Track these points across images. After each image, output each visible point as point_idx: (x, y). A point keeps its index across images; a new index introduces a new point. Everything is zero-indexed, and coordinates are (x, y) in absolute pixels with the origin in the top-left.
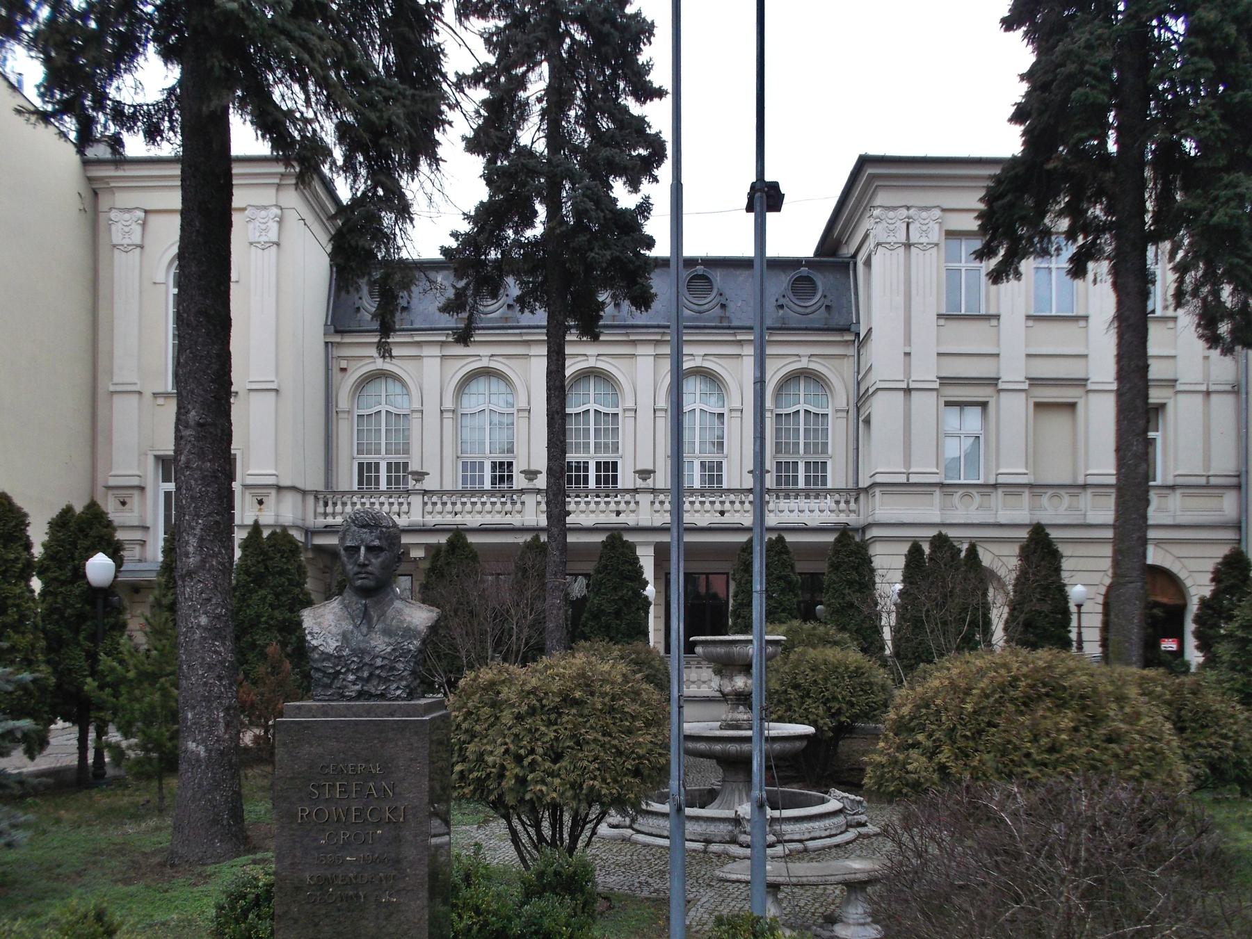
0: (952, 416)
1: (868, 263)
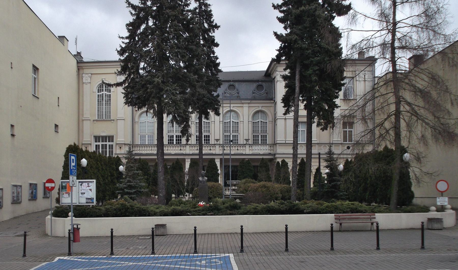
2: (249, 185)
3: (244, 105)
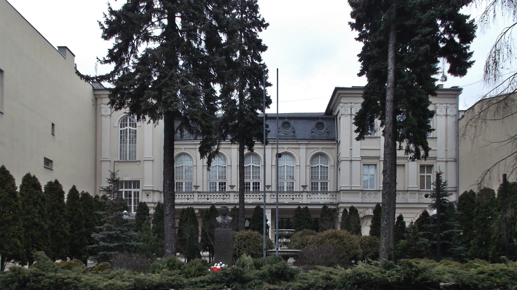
0: (366, 169)
1: (340, 118)
2: (308, 237)
3: (301, 146)
